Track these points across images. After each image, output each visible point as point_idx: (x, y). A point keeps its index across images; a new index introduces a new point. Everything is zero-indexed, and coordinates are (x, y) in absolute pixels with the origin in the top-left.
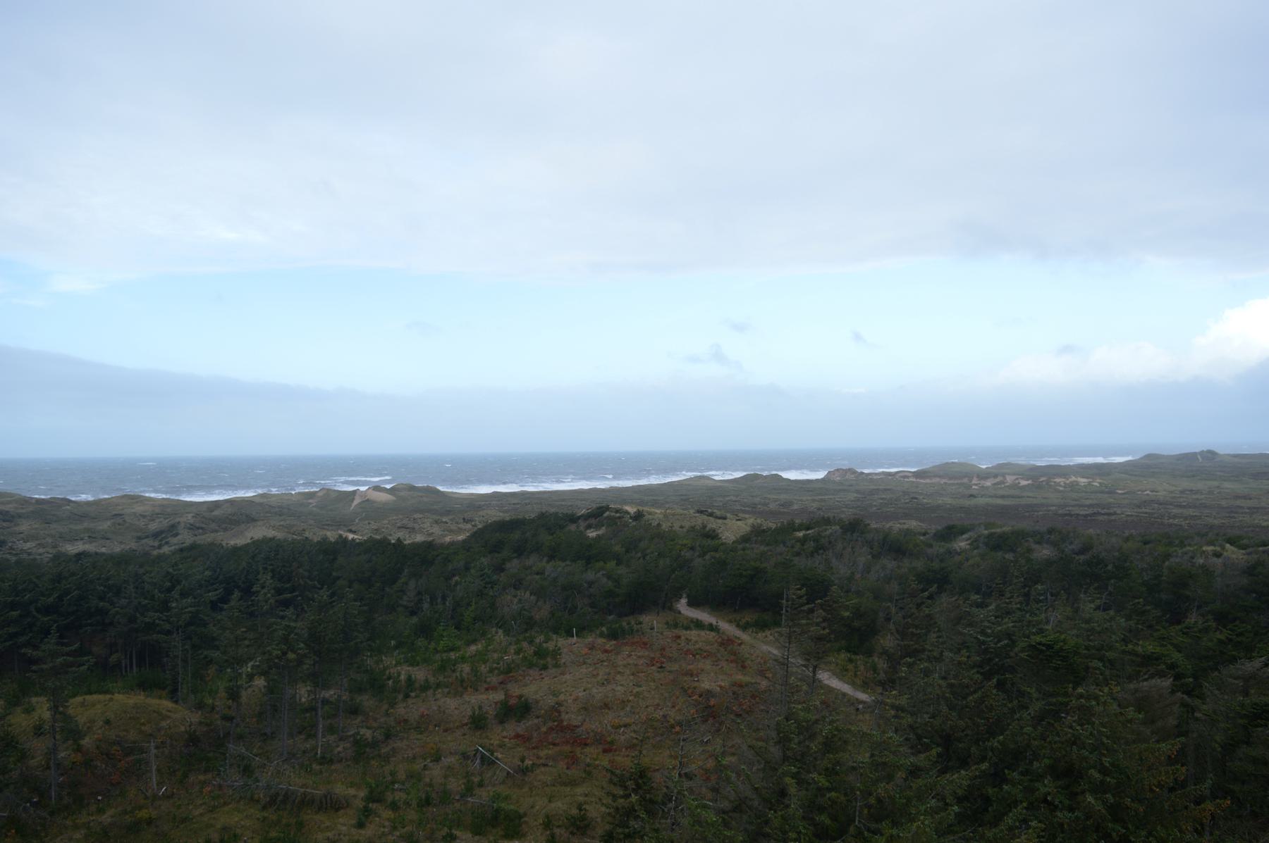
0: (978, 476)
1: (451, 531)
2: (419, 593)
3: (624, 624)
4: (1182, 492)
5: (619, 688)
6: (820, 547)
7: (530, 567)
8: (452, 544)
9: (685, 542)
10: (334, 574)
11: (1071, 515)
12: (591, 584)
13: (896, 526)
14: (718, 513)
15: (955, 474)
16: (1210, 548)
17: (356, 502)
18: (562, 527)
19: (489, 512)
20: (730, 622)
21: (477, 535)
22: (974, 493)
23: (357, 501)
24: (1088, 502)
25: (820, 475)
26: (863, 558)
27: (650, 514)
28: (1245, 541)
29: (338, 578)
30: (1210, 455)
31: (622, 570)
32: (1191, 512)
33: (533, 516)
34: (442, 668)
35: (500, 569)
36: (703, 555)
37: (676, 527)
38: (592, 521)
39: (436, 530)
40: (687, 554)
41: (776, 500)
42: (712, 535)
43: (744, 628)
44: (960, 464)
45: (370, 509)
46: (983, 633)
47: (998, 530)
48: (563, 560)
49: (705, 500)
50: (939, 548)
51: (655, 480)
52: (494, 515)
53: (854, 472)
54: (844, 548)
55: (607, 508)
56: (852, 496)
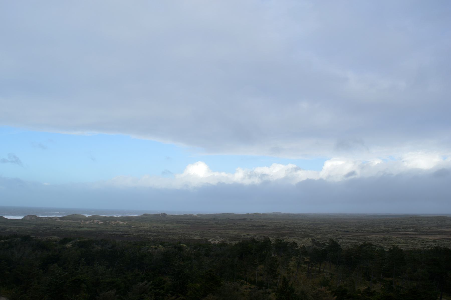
0: (84, 220)
4: (153, 227)
11: (115, 235)
15: (75, 218)
16: (154, 246)
22: (81, 226)
24: (122, 230)
25: (21, 217)
28: (166, 244)
30: (164, 215)
32: (155, 234)
47: (83, 240)
53: (36, 217)
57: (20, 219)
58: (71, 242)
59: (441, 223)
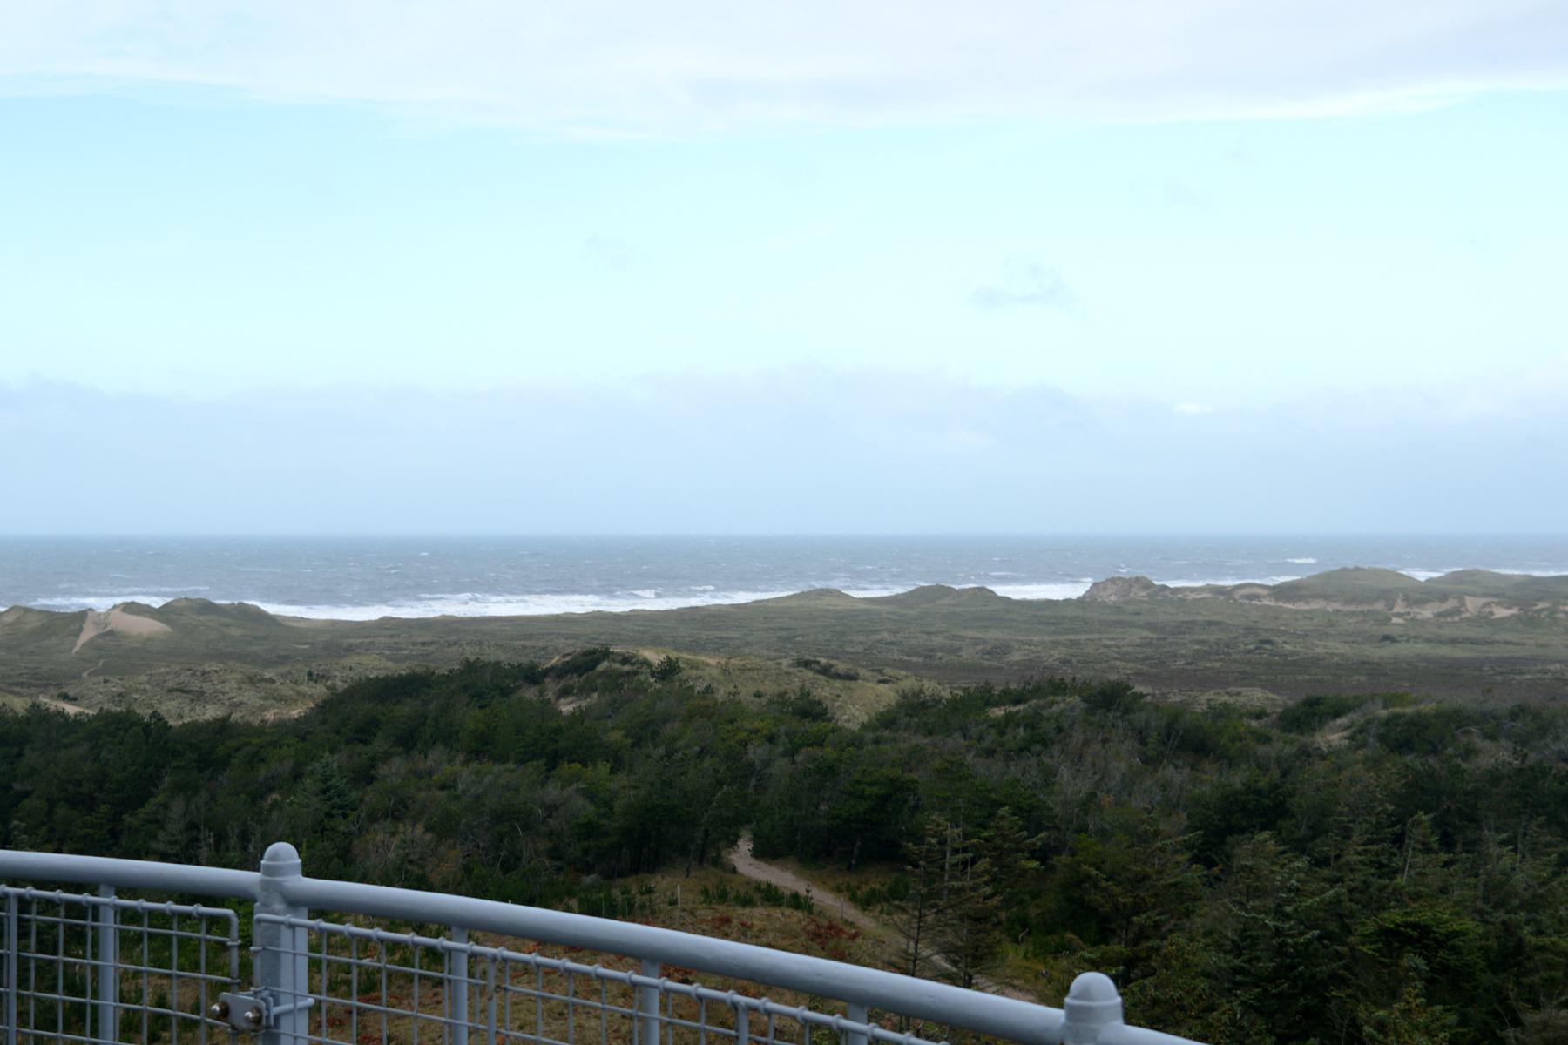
0: (1406, 599)
1: (281, 699)
2: (192, 826)
3: (616, 893)
5: (593, 1023)
6: (1038, 737)
7: (430, 773)
8: (280, 725)
9: (757, 724)
10: (17, 786)
12: (551, 809)
13: (1204, 699)
14: (841, 667)
15: (1359, 590)
17: (84, 637)
18: (505, 692)
19: (365, 660)
20: (838, 890)
21: (326, 707)
23: (88, 634)
25: (1074, 591)
26: (1122, 760)
27: (693, 666)
29: (27, 794)
31: (621, 780)
33: (443, 671)
34: (1250, 961)
35: (365, 776)
36: (791, 753)
37: (746, 693)
38: (573, 680)
39: (250, 697)
40: (756, 752)
41: (976, 642)
42: (811, 710)
43: (865, 903)
44: (1375, 572)
45: (114, 652)
46: (1279, 913)
47: (1409, 710)
48: (502, 759)
49: (820, 639)
50: (1282, 746)
51: (651, 602)
52: (375, 665)
53: (1148, 585)
54: (1086, 743)
55: (606, 654)
56: (1136, 636)
57: (1067, 601)
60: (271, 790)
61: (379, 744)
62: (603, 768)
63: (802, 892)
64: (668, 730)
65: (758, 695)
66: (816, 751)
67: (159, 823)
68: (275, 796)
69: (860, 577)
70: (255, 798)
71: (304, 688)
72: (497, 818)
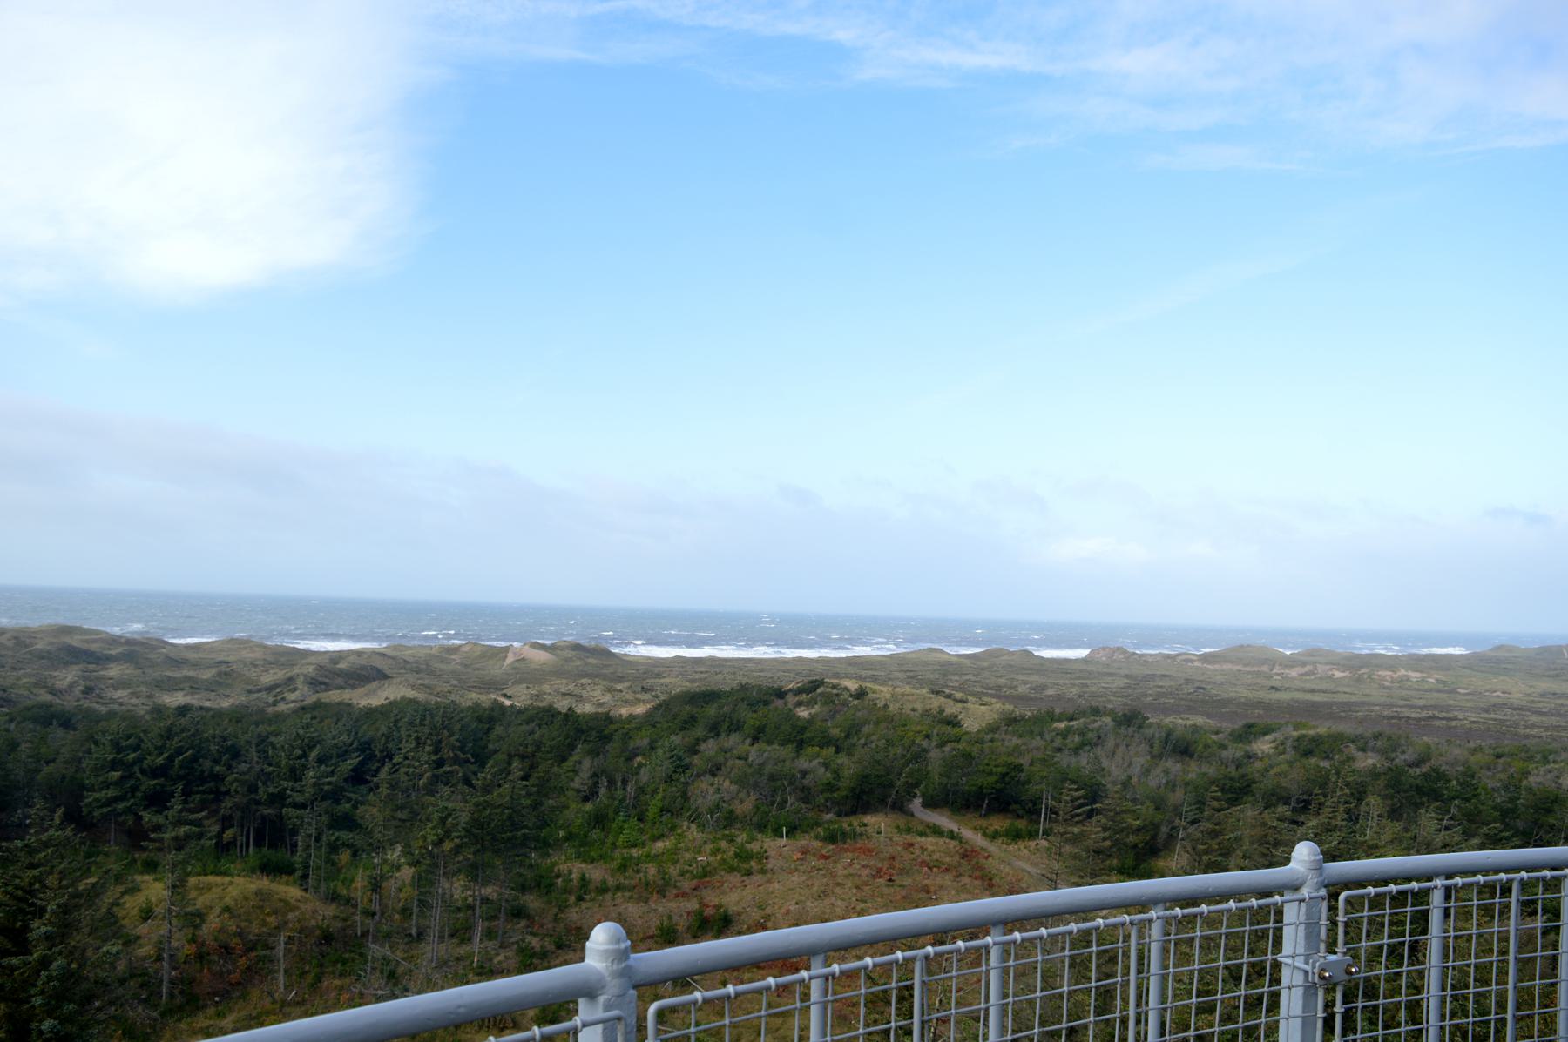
2: (595, 775)
3: (845, 825)
4: (1543, 695)
6: (1089, 742)
10: (491, 746)
12: (804, 773)
23: (510, 659)
24: (1422, 702)
25: (1082, 653)
29: (496, 751)
32: (1554, 721)
35: (693, 750)
38: (804, 697)
45: (525, 673)
47: (1311, 732)
48: (770, 743)
49: (942, 676)
50: (1234, 751)
52: (677, 684)
53: (1125, 652)
54: (1117, 746)
55: (822, 683)
56: (1123, 682)
57: (1077, 660)
58: (1267, 738)
59: (1553, 661)
60: (636, 755)
61: (699, 731)
62: (832, 750)
63: (955, 829)
64: (866, 730)
65: (913, 710)
66: (955, 745)
67: (575, 772)
68: (639, 759)
69: (950, 643)
70: (630, 759)
71: (639, 696)
72: (772, 778)
